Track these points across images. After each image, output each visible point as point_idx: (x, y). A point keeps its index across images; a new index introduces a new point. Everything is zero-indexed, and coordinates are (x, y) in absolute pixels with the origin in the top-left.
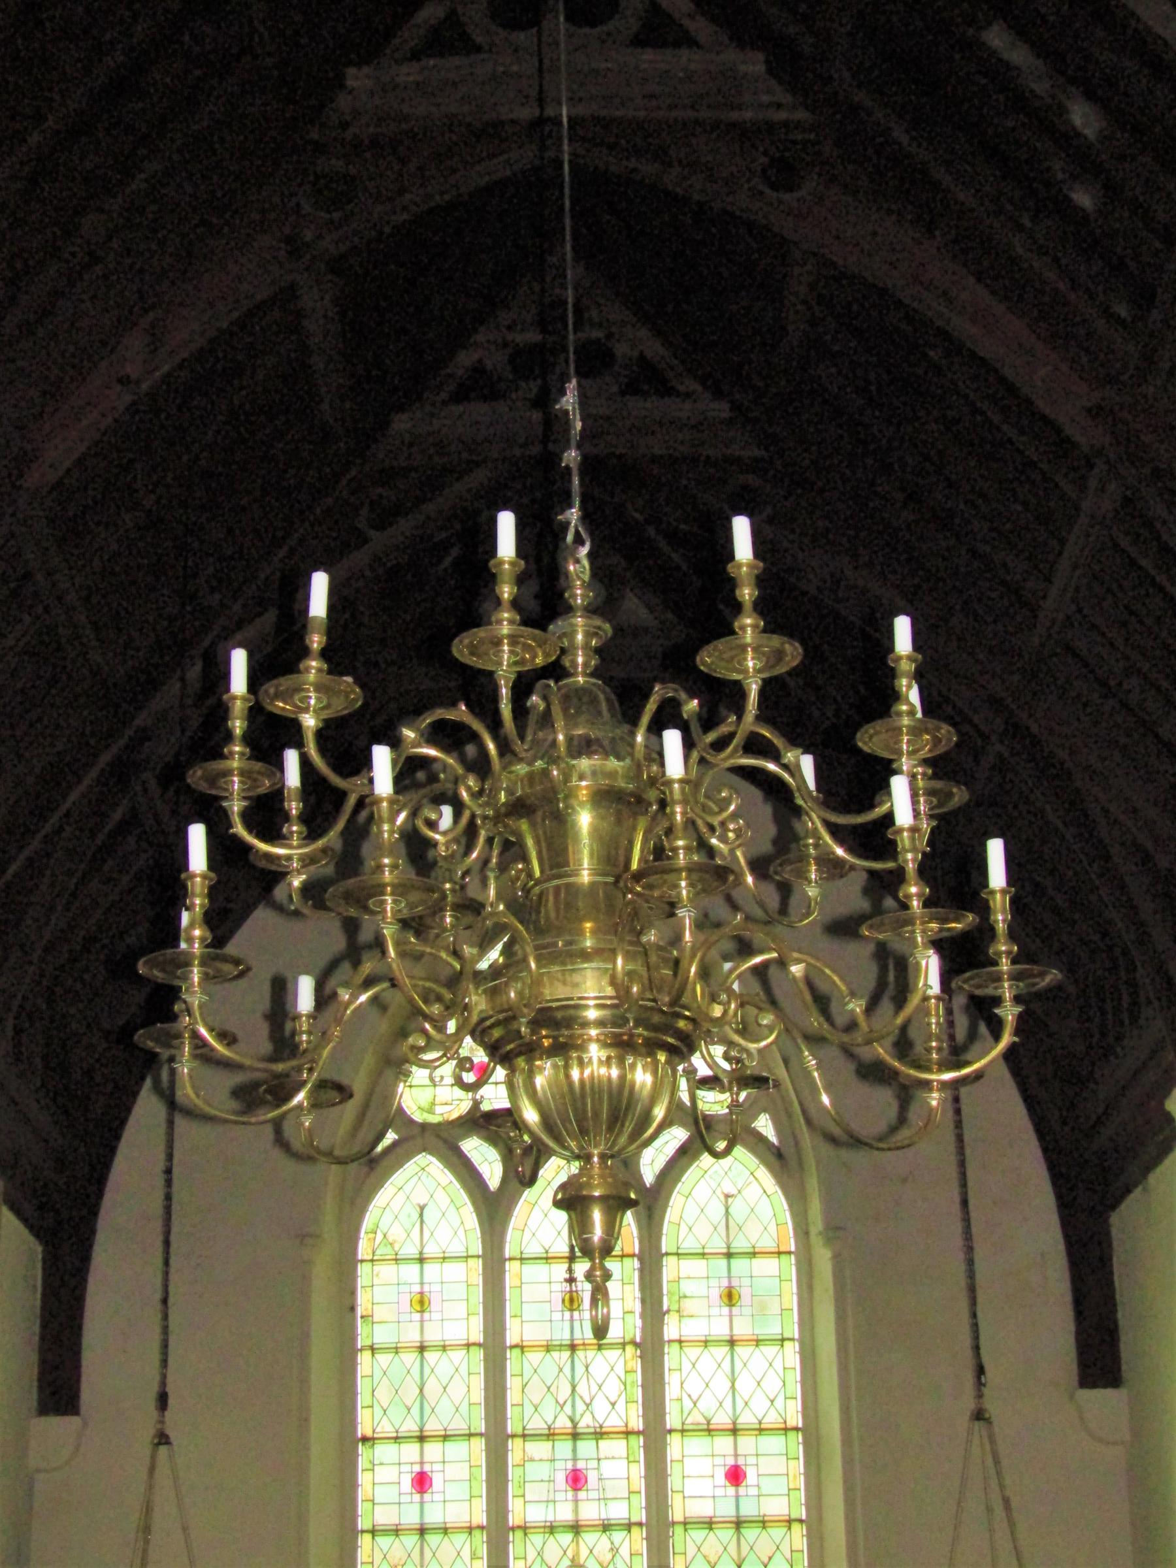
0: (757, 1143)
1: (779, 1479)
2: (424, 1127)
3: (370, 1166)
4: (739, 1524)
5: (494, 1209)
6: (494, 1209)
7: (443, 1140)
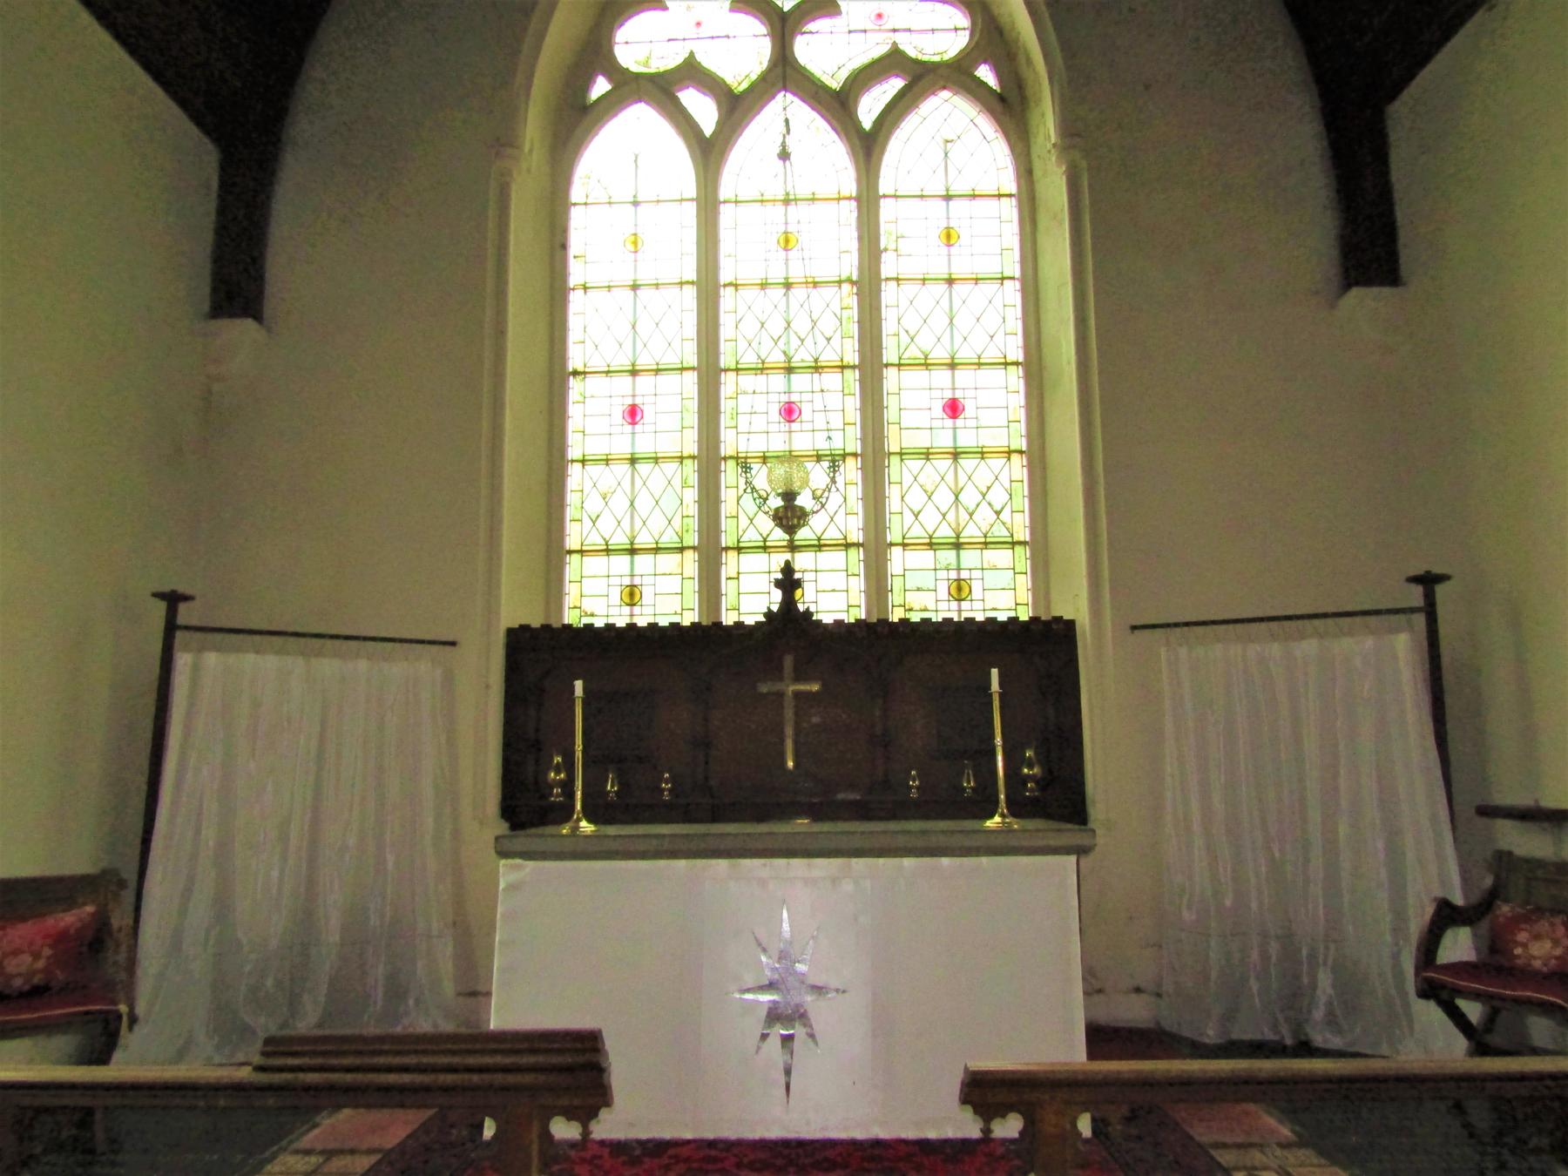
0: (975, 90)
1: (999, 406)
2: (638, 77)
3: (575, 120)
4: (956, 455)
5: (709, 152)
7: (661, 89)
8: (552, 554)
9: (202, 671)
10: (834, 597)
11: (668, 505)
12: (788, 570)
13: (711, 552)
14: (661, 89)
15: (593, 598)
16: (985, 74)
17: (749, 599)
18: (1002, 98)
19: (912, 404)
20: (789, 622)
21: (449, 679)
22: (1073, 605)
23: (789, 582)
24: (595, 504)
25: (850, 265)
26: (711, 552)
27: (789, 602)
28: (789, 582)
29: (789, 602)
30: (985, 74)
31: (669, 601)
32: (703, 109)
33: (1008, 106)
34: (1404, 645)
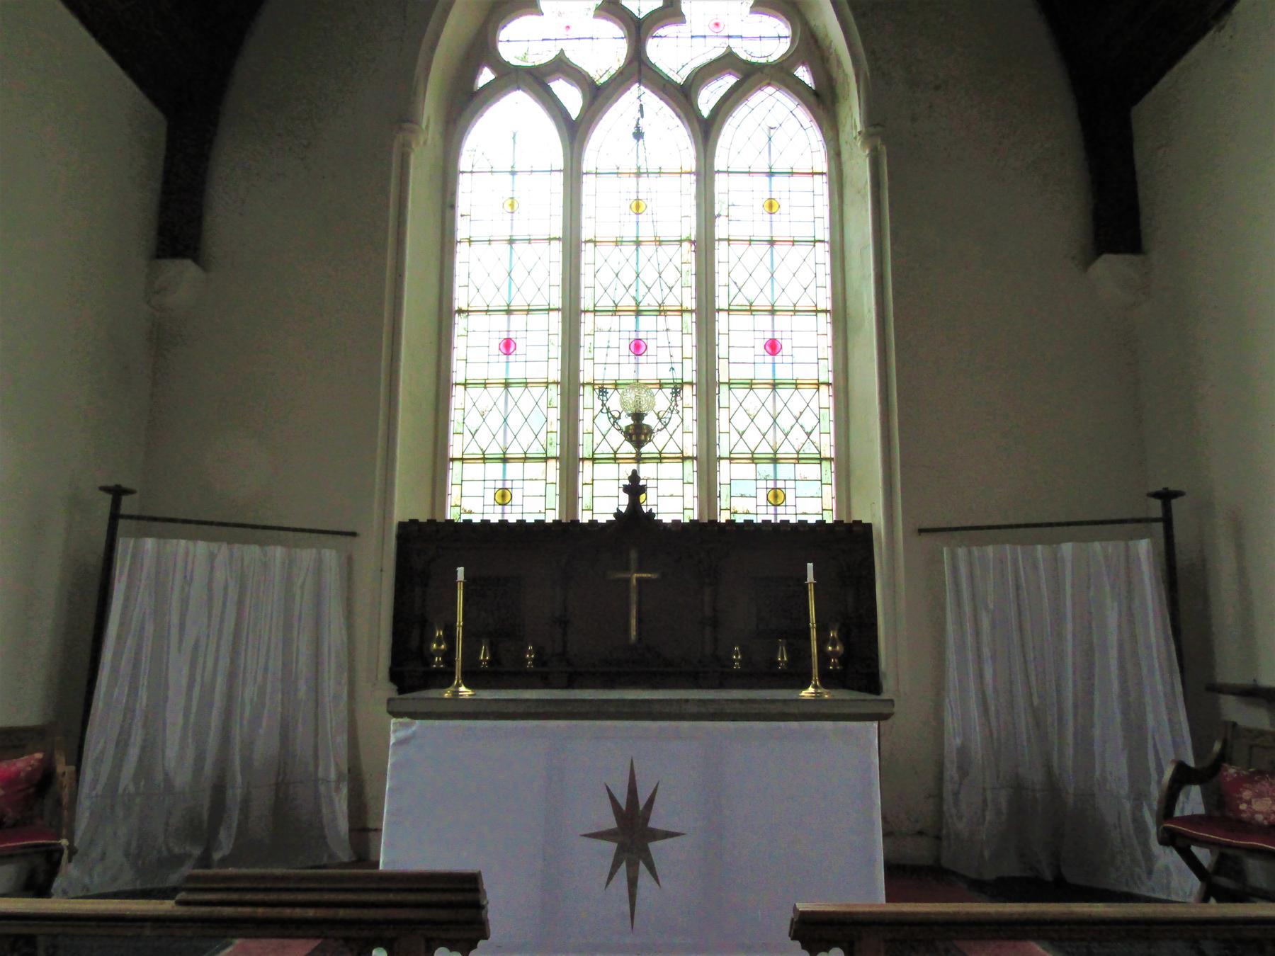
0: (795, 87)
1: (811, 346)
3: (464, 103)
5: (575, 132)
6: (575, 132)
7: (536, 80)
8: (439, 462)
9: (140, 554)
10: (672, 501)
11: (536, 422)
12: (634, 477)
13: (570, 462)
14: (536, 80)
15: (471, 498)
16: (803, 74)
17: (602, 502)
18: (816, 94)
19: (739, 342)
20: (635, 521)
21: (349, 565)
22: (870, 509)
23: (635, 488)
24: (473, 420)
25: (689, 228)
26: (570, 462)
27: (635, 504)
28: (635, 488)
29: (635, 504)
30: (803, 74)
31: (536, 502)
32: (571, 97)
33: (822, 102)
34: (1144, 548)
